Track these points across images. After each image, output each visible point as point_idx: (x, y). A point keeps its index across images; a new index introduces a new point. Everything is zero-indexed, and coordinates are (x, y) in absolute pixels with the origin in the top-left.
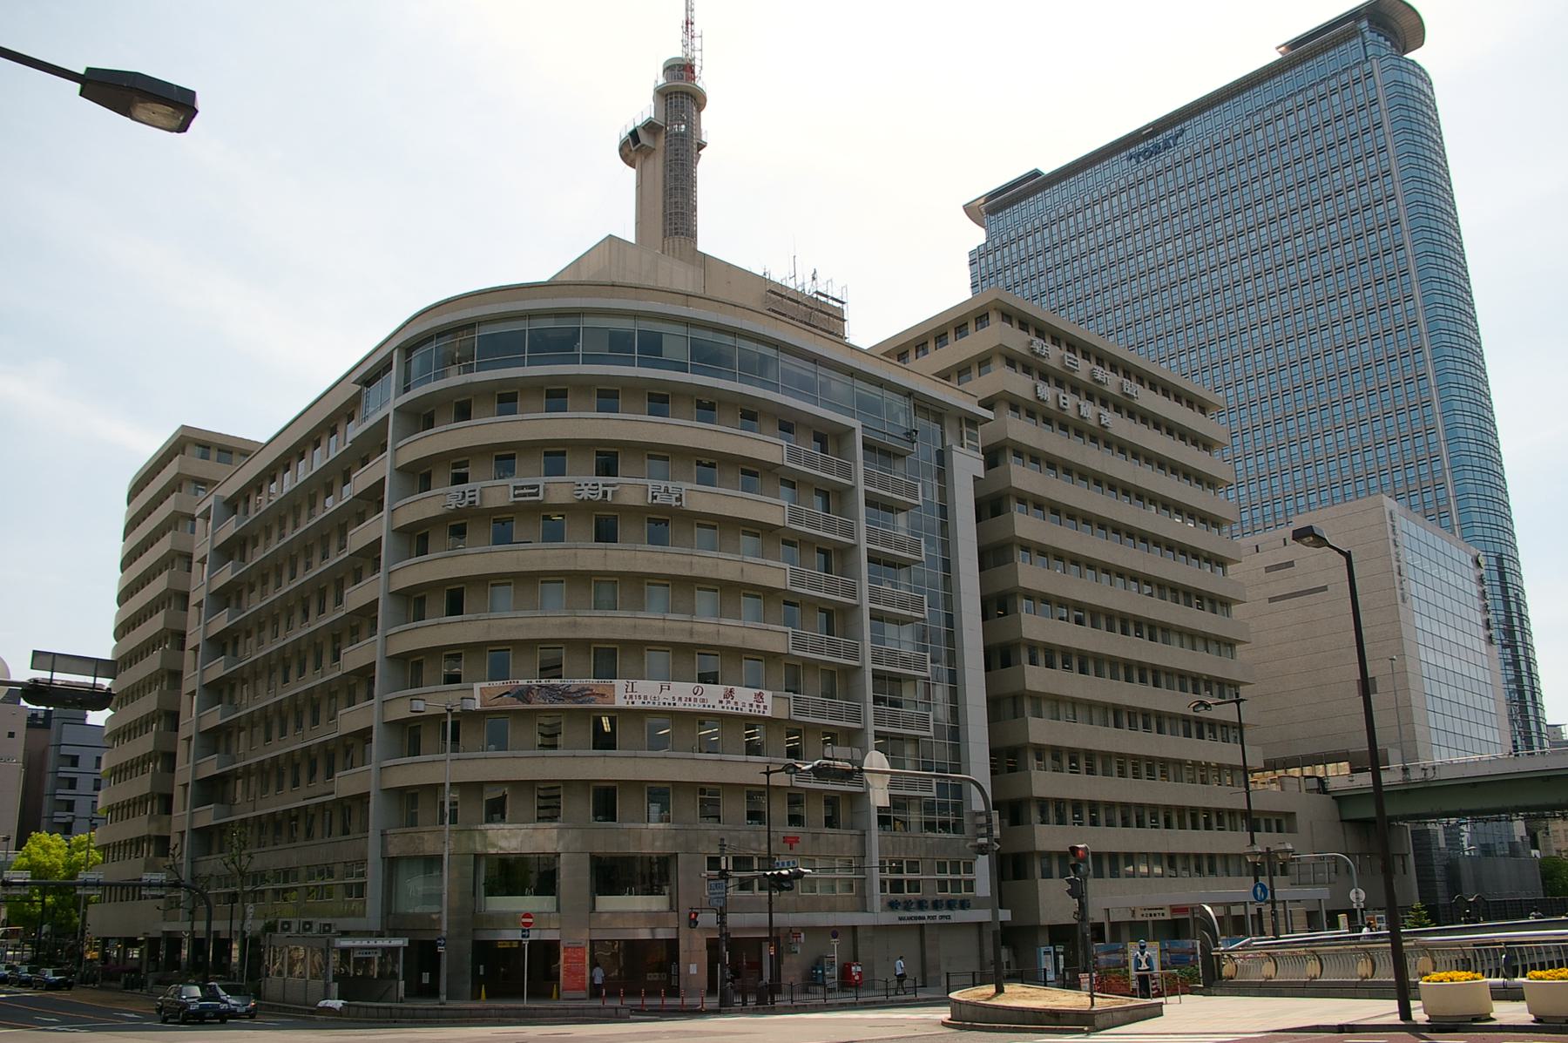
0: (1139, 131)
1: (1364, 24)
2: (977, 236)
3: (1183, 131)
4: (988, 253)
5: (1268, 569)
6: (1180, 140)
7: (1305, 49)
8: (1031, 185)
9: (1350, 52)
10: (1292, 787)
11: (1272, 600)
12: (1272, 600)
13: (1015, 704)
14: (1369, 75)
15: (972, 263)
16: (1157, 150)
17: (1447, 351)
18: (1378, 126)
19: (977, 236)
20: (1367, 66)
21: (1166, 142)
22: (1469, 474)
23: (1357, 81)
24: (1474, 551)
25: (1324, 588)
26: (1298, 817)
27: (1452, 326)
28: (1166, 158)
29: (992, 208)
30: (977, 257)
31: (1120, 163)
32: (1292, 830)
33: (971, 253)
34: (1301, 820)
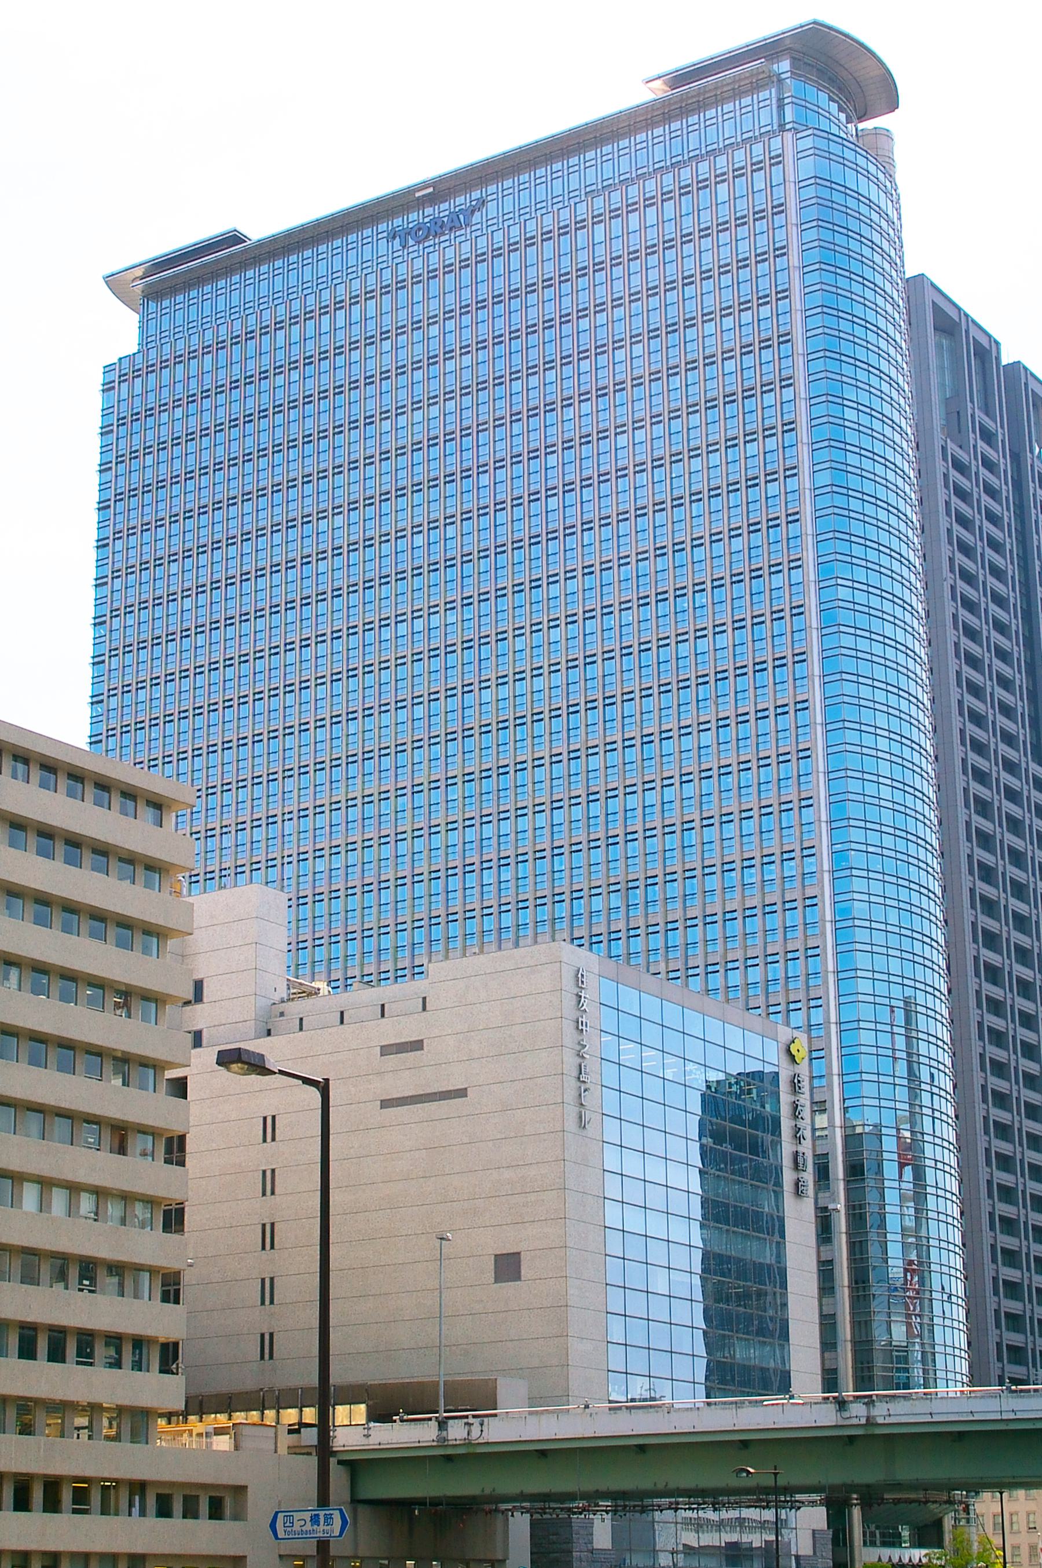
0: (303, 229)
1: (785, 65)
2: (120, 331)
3: (483, 202)
4: (137, 373)
5: (386, 1050)
6: (476, 218)
7: (695, 89)
8: (218, 260)
9: (758, 111)
10: (259, 1442)
11: (385, 1104)
12: (385, 1104)
13: (861, 1246)
14: (777, 160)
15: (107, 388)
16: (437, 229)
17: (848, 665)
18: (781, 251)
19: (120, 331)
20: (776, 143)
21: (454, 216)
22: (858, 884)
23: (757, 167)
24: (784, 1033)
25: (462, 1093)
26: (250, 1491)
27: (862, 621)
28: (450, 249)
29: (169, 281)
30: (118, 377)
31: (374, 245)
32: (238, 1516)
33: (108, 369)
34: (259, 1506)
